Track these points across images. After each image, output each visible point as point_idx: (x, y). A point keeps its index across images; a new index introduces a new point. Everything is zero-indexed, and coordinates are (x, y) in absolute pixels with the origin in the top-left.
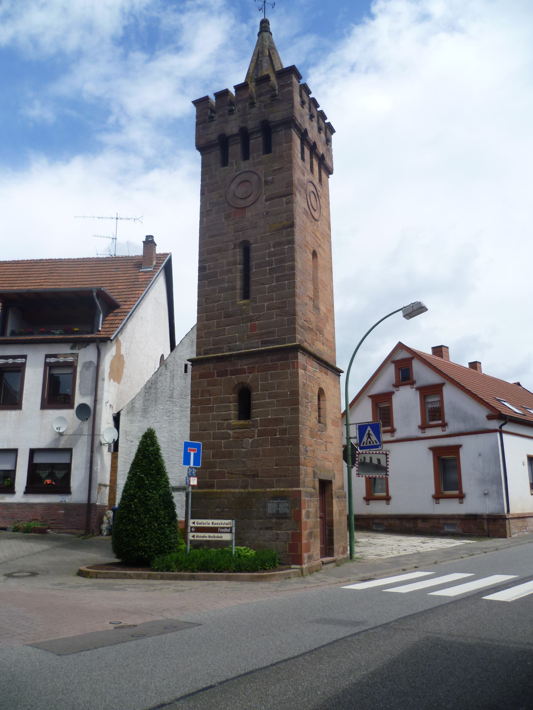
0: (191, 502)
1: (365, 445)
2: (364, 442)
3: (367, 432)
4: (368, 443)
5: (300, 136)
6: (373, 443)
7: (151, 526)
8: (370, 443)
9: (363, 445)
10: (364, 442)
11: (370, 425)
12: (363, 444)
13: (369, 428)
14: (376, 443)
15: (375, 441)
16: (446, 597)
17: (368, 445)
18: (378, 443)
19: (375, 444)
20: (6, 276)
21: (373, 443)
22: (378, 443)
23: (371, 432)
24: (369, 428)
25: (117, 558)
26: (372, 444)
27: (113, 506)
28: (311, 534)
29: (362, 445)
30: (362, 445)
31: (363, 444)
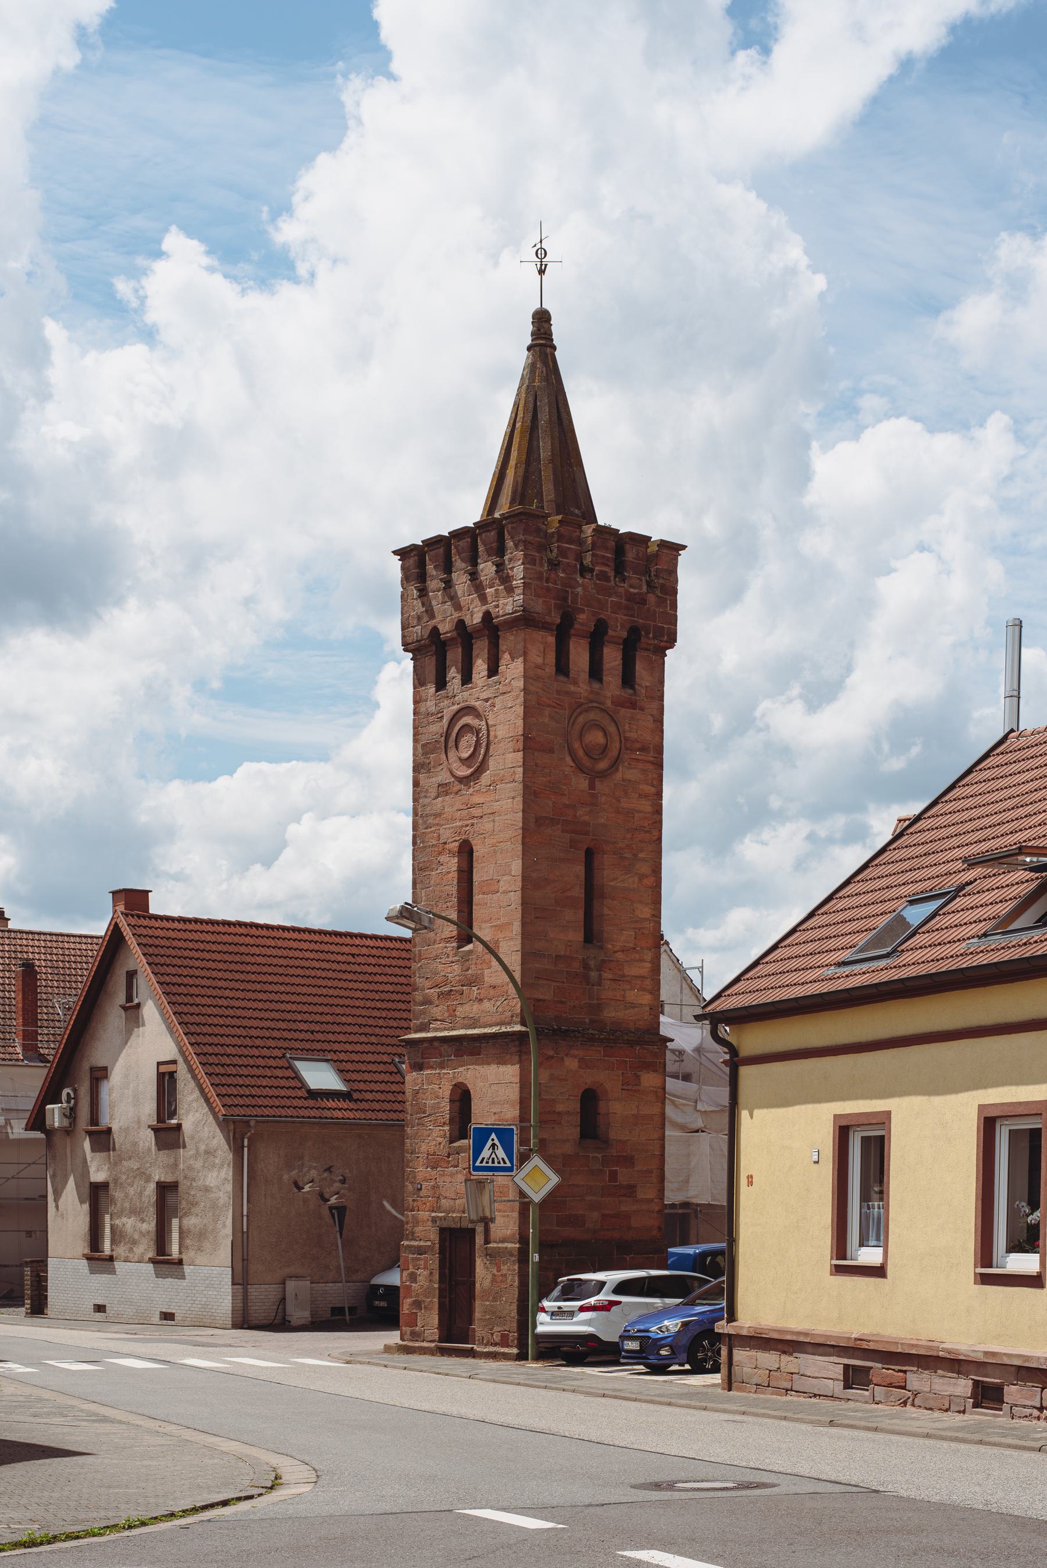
0: (871, 1098)
1: (484, 1164)
2: (483, 1159)
3: (490, 1143)
4: (490, 1160)
5: (535, 615)
6: (499, 1163)
7: (37, 1044)
8: (493, 1162)
9: (481, 1165)
10: (483, 1159)
11: (496, 1131)
12: (481, 1162)
13: (493, 1136)
14: (505, 1163)
15: (503, 1159)
16: (535, 1517)
17: (490, 1164)
18: (509, 1164)
19: (502, 1164)
20: (272, 997)
21: (499, 1163)
22: (509, 1164)
23: (496, 1142)
24: (493, 1136)
25: (445, 574)
26: (496, 1164)
27: (265, 213)
28: (417, 1304)
29: (478, 1164)
30: (478, 1164)
31: (481, 1162)
